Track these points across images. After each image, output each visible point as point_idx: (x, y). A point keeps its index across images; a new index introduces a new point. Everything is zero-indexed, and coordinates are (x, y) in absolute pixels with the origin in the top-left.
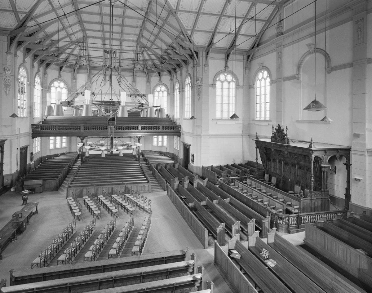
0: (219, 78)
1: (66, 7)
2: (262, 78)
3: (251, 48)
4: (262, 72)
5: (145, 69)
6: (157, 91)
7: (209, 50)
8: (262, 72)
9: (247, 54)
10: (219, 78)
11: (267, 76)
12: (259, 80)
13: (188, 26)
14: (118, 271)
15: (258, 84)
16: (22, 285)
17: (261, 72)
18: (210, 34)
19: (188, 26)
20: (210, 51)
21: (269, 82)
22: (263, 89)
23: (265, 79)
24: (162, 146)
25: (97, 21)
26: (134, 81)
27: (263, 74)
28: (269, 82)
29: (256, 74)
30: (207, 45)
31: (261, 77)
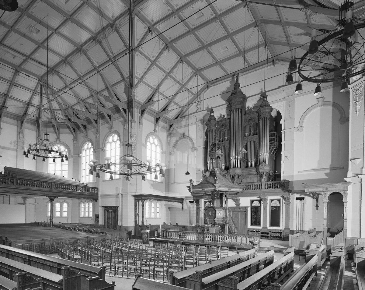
0: (60, 146)
1: (161, 32)
2: (113, 141)
3: (147, 101)
4: (113, 135)
5: (235, 76)
6: (109, 143)
7: (24, 120)
8: (87, 143)
9: (141, 108)
10: (60, 146)
11: (118, 140)
12: (88, 150)
13: (138, 73)
14: (219, 272)
15: (108, 147)
16: (330, 148)
17: (112, 136)
18: (116, 88)
19: (138, 73)
20: (25, 120)
21: (119, 144)
22: (113, 151)
23: (89, 149)
24: (61, 216)
25: (213, 46)
26: (20, 132)
27: (88, 145)
28: (119, 144)
29: (82, 146)
30: (22, 115)
31: (112, 140)
